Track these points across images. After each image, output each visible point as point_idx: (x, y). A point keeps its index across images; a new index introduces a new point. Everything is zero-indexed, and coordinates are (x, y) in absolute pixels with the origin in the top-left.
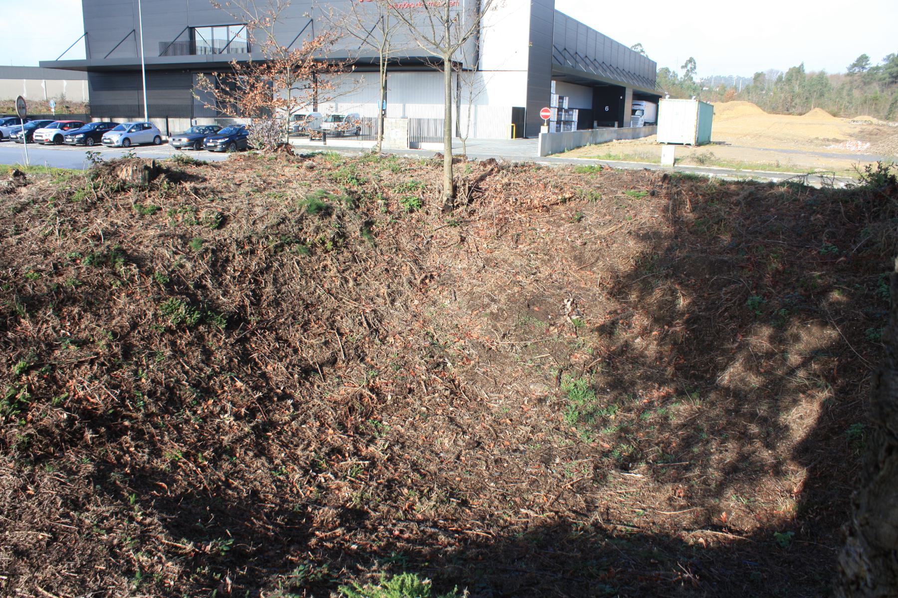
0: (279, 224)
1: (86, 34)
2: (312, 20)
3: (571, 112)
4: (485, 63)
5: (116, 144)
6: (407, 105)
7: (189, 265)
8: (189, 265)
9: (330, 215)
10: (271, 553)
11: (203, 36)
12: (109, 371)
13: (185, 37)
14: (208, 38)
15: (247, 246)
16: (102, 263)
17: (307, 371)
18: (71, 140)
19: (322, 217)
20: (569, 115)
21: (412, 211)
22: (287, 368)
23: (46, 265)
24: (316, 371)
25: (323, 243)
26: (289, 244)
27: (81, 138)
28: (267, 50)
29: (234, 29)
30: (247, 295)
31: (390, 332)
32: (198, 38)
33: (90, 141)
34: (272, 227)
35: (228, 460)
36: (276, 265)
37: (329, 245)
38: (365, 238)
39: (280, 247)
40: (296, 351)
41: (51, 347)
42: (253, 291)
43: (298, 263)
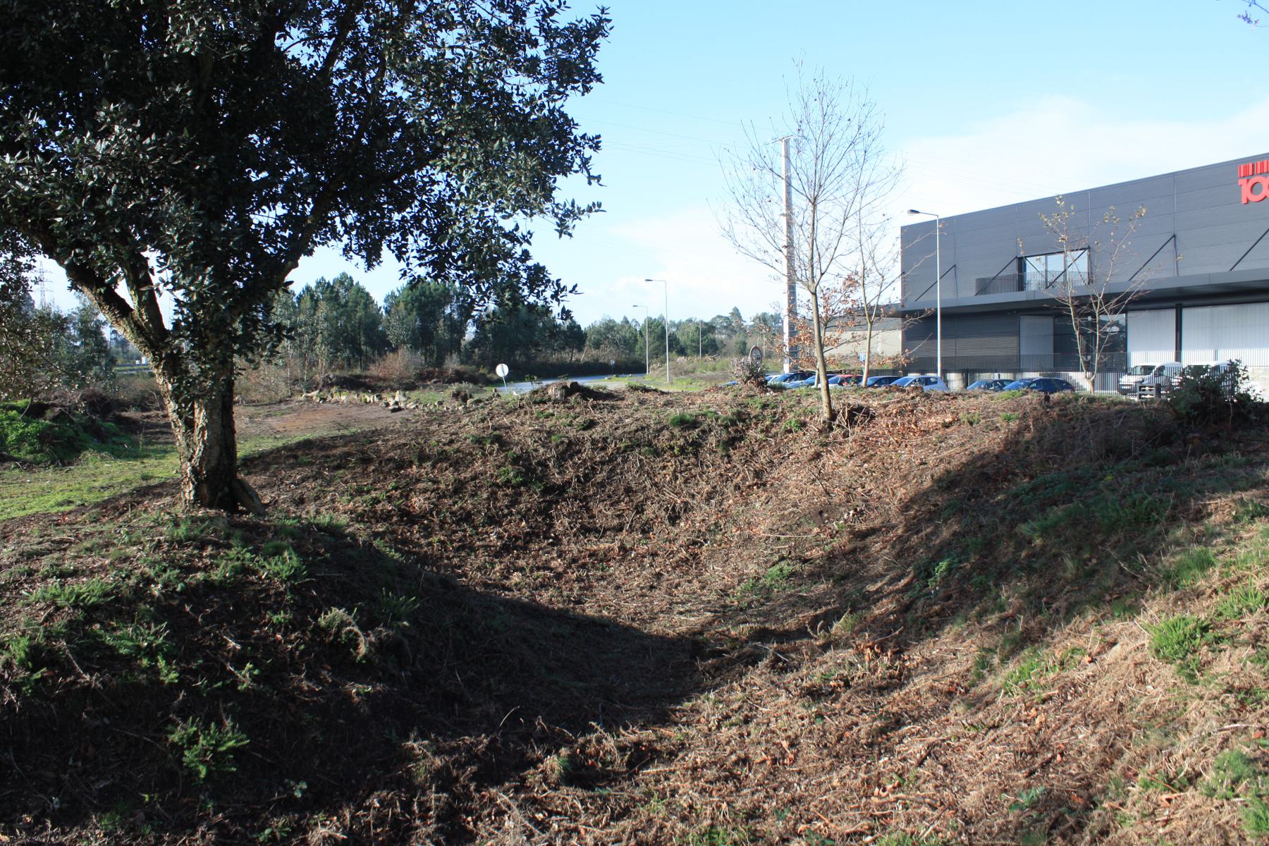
0: (636, 431)
1: (903, 273)
6: (1186, 312)
7: (541, 450)
11: (1035, 268)
13: (1013, 270)
14: (1042, 269)
16: (856, 410)
17: (586, 530)
19: (683, 430)
21: (790, 431)
22: (570, 523)
24: (599, 532)
25: (672, 448)
26: (638, 446)
34: (630, 433)
36: (619, 460)
38: (719, 450)
39: (630, 448)
40: (593, 517)
41: (418, 481)
42: (586, 476)
43: (641, 460)
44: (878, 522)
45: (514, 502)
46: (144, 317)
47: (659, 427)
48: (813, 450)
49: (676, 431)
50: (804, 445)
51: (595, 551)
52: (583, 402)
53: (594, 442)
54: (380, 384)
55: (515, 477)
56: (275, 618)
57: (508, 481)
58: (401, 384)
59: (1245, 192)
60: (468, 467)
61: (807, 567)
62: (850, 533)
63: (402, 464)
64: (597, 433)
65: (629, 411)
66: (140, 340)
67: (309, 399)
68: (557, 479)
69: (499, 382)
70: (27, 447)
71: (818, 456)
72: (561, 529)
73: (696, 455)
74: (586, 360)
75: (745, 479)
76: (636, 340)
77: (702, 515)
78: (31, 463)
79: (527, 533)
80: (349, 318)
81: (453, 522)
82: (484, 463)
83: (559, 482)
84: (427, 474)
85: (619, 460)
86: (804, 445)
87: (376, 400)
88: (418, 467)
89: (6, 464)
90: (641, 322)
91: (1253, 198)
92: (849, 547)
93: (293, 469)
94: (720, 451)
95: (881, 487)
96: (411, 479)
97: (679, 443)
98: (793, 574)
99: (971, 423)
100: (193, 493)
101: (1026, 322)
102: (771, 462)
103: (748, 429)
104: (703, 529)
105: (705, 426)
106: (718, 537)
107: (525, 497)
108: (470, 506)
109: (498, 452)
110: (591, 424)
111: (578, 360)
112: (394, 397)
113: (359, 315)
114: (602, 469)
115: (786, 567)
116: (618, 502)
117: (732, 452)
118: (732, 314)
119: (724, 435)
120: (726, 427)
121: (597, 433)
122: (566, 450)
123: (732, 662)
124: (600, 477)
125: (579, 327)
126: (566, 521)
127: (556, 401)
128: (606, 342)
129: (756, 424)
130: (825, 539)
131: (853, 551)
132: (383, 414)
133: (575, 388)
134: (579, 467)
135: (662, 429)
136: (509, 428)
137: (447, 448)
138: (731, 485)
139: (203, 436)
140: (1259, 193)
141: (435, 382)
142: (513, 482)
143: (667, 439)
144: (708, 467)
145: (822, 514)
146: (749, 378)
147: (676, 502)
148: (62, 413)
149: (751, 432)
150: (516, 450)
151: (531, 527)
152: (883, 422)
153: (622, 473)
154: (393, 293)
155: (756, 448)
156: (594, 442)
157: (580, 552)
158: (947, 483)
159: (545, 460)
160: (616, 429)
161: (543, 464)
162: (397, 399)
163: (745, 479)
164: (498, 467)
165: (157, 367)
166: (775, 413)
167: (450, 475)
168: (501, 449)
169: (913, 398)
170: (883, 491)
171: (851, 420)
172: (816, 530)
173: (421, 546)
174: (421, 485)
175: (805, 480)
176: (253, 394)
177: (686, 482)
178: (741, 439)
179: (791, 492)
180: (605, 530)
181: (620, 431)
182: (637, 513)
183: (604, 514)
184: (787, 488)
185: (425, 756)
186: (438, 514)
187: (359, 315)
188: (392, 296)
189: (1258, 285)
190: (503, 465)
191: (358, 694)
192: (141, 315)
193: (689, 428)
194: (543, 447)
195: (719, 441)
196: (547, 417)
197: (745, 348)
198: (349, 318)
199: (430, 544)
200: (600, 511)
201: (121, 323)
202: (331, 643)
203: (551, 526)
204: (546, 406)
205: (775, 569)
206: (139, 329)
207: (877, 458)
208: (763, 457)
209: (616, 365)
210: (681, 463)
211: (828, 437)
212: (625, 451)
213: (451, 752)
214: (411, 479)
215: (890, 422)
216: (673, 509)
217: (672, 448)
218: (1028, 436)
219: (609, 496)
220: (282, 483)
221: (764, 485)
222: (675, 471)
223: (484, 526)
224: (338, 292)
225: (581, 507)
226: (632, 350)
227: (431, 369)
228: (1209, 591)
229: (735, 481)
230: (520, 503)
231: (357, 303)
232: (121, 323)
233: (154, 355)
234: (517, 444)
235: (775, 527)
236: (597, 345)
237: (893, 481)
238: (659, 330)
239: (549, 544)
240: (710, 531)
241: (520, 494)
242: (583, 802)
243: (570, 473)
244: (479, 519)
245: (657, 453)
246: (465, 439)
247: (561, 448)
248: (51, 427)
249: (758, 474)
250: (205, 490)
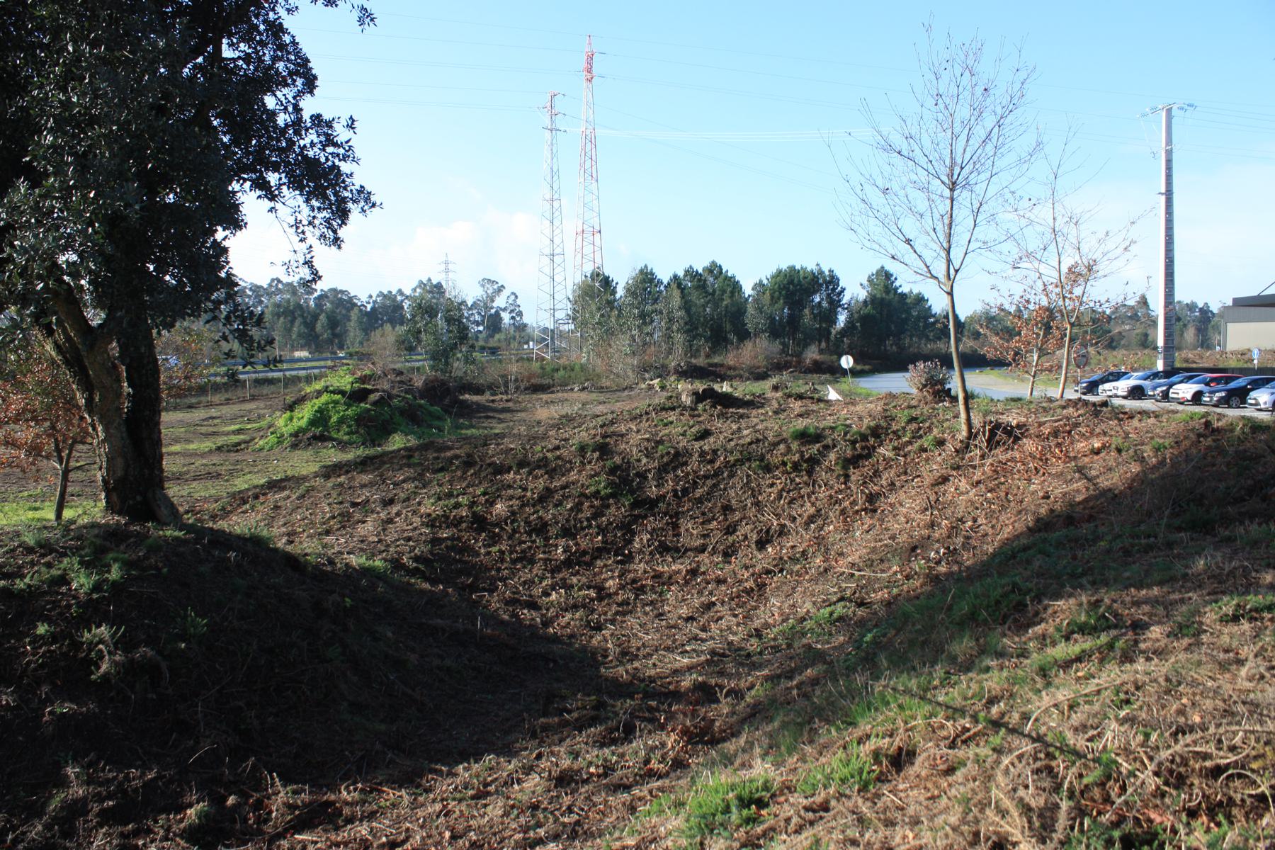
0: (750, 444)
5: (1262, 406)
7: (644, 460)
15: (708, 457)
17: (664, 549)
18: (1208, 399)
21: (925, 450)
22: (648, 541)
25: (784, 464)
26: (749, 460)
27: (1222, 398)
31: (1235, 644)
33: (1234, 401)
34: (743, 445)
35: (789, 646)
36: (726, 474)
39: (739, 462)
41: (510, 487)
43: (748, 476)
49: (795, 446)
50: (935, 465)
53: (702, 454)
55: (605, 488)
57: (598, 492)
58: (751, 373)
61: (861, 612)
63: (501, 470)
64: (708, 444)
67: (651, 387)
68: (653, 492)
69: (844, 372)
70: (345, 428)
75: (854, 503)
77: (798, 539)
78: (346, 443)
80: (716, 306)
81: (526, 532)
85: (726, 474)
88: (515, 473)
89: (326, 444)
103: (879, 446)
105: (829, 441)
107: (612, 510)
109: (597, 460)
110: (705, 434)
113: (725, 303)
115: (839, 609)
116: (709, 521)
120: (854, 443)
121: (708, 444)
122: (671, 461)
124: (699, 492)
126: (646, 537)
133: (709, 394)
134: (680, 480)
135: (779, 443)
141: (791, 372)
146: (925, 386)
148: (382, 398)
149: (882, 450)
150: (617, 460)
153: (725, 489)
154: (761, 281)
159: (646, 471)
161: (642, 476)
167: (541, 484)
168: (600, 458)
171: (992, 443)
173: (478, 554)
174: (510, 492)
176: (604, 380)
177: (790, 503)
180: (687, 550)
186: (512, 522)
187: (725, 303)
188: (760, 284)
190: (597, 474)
193: (810, 443)
194: (647, 457)
198: (716, 306)
199: (489, 553)
200: (687, 530)
210: (792, 481)
211: (963, 459)
212: (734, 465)
216: (768, 531)
217: (784, 464)
219: (703, 514)
221: (875, 511)
223: (556, 538)
224: (705, 280)
231: (724, 292)
241: (608, 506)
244: (553, 531)
245: (768, 469)
247: (665, 460)
248: (369, 410)
249: (872, 498)
250: (115, 497)
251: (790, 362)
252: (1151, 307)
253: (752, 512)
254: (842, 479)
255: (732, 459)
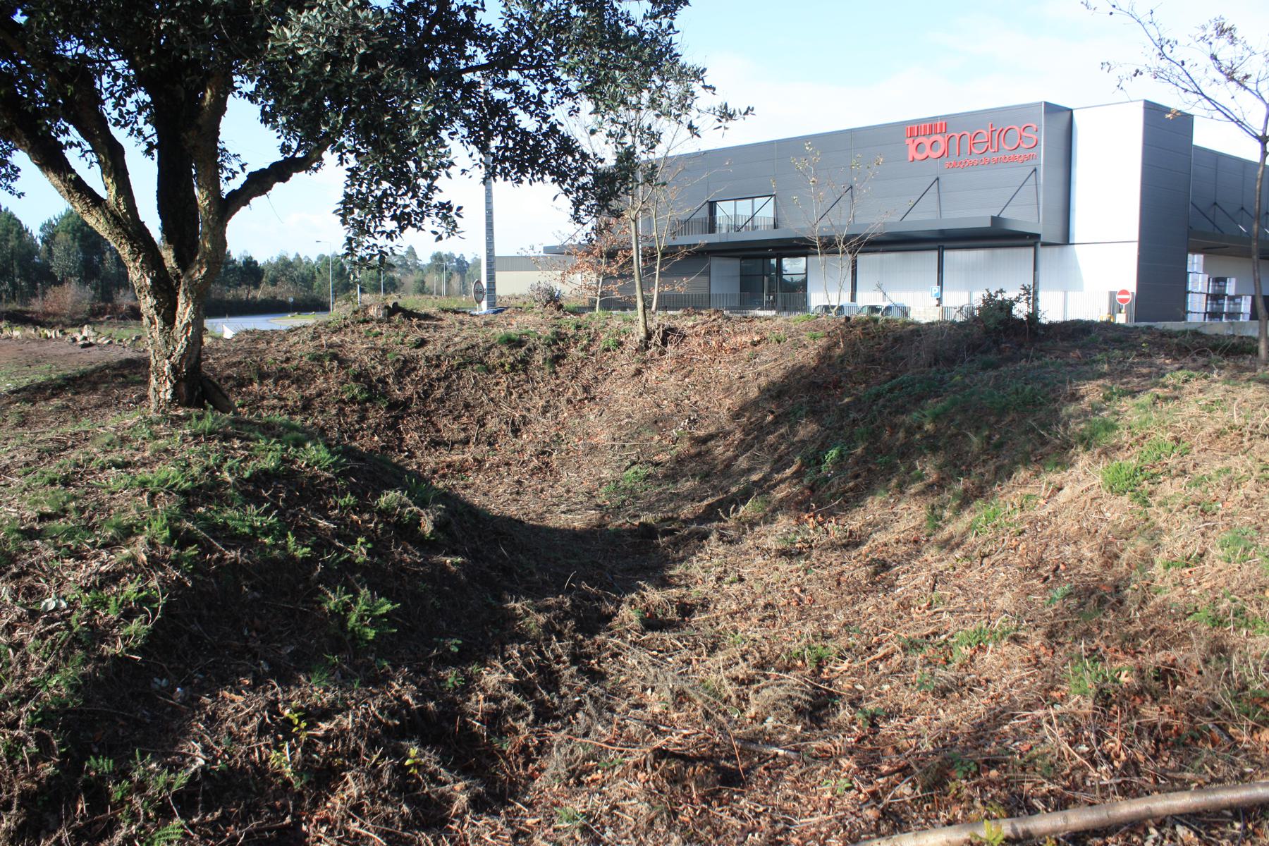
0: (467, 349)
2: (938, 179)
3: (1237, 300)
4: (1078, 233)
7: (379, 368)
8: (379, 368)
9: (521, 347)
10: (530, 821)
11: (725, 210)
12: (289, 414)
13: (704, 213)
15: (434, 361)
17: (436, 444)
19: (511, 348)
20: (1235, 304)
21: (608, 350)
22: (420, 437)
23: (281, 357)
24: (448, 445)
25: (503, 365)
26: (471, 363)
28: (794, 228)
29: (759, 202)
30: (417, 393)
32: (719, 213)
34: (461, 351)
36: (454, 376)
37: (507, 368)
38: (546, 367)
39: (463, 365)
40: (438, 431)
41: (263, 398)
42: (425, 392)
43: (474, 377)
44: (712, 429)
45: (363, 419)
46: (122, 207)
47: (487, 345)
48: (633, 366)
49: (505, 349)
50: (624, 363)
51: (450, 463)
52: (407, 322)
53: (428, 359)
54: (49, 319)
55: (361, 393)
56: (341, 502)
59: (912, 148)
60: (310, 384)
61: (660, 470)
62: (691, 439)
64: (429, 350)
65: (455, 331)
66: (118, 231)
68: (398, 394)
71: (639, 372)
72: (412, 442)
73: (525, 371)
74: (263, 297)
76: (314, 278)
77: (541, 427)
79: (383, 447)
82: (326, 380)
83: (401, 398)
84: (270, 391)
85: (454, 376)
86: (623, 362)
87: (59, 335)
90: (314, 259)
91: (919, 156)
92: (692, 451)
93: (126, 387)
94: (548, 369)
95: (706, 399)
96: (256, 396)
97: (509, 360)
98: (648, 476)
99: (779, 342)
100: (170, 392)
101: (715, 263)
102: (596, 378)
104: (547, 440)
105: (529, 345)
106: (564, 447)
107: (371, 414)
108: (322, 422)
109: (338, 369)
110: (422, 343)
111: (254, 298)
112: (81, 333)
113: (11, 244)
114: (439, 386)
116: (460, 416)
117: (558, 369)
118: (407, 252)
119: (549, 353)
121: (429, 350)
123: (686, 539)
124: (439, 393)
125: (256, 263)
127: (379, 321)
128: (283, 279)
129: (575, 343)
130: (667, 446)
131: (699, 454)
132: (71, 350)
135: (491, 347)
136: (340, 346)
137: (285, 365)
138: (564, 400)
139: (187, 333)
140: (921, 153)
141: (109, 319)
142: (359, 398)
143: (498, 357)
144: (538, 383)
145: (659, 423)
146: (548, 302)
147: (514, 416)
149: (572, 351)
150: (355, 366)
151: (383, 441)
152: (694, 342)
154: (50, 221)
155: (579, 365)
156: (428, 359)
157: (437, 464)
158: (776, 392)
160: (447, 347)
161: (382, 381)
162: (85, 334)
163: (575, 394)
164: (342, 384)
165: (134, 260)
166: (589, 334)
169: (714, 320)
170: (709, 402)
172: (657, 438)
175: (632, 394)
177: (520, 396)
178: (564, 357)
179: (622, 405)
180: (453, 443)
181: (451, 349)
182: (481, 426)
183: (450, 429)
184: (616, 401)
185: (527, 614)
187: (11, 244)
188: (50, 224)
189: (923, 235)
191: (452, 563)
192: (118, 204)
195: (545, 359)
196: (376, 336)
197: (423, 287)
200: (445, 425)
201: (94, 212)
202: (395, 523)
203: (402, 440)
204: (371, 325)
205: (630, 472)
206: (116, 220)
207: (696, 373)
208: (587, 373)
209: (294, 303)
210: (513, 380)
212: (458, 369)
213: (548, 609)
214: (256, 396)
215: (702, 342)
217: (503, 365)
218: (838, 351)
220: (119, 402)
221: (594, 398)
222: (508, 387)
225: (426, 422)
226: (310, 287)
227: (102, 304)
228: (1127, 445)
229: (566, 396)
230: (368, 419)
232: (94, 212)
233: (132, 246)
234: (354, 362)
235: (616, 436)
236: (274, 282)
237: (716, 393)
238: (337, 267)
239: (406, 457)
240: (554, 441)
241: (367, 410)
242: (678, 639)
243: (410, 390)
245: (489, 371)
246: (301, 357)
249: (586, 389)
250: (183, 389)
251: (105, 308)
252: (419, 257)
253: (491, 407)
254: (554, 376)
255: (455, 363)
